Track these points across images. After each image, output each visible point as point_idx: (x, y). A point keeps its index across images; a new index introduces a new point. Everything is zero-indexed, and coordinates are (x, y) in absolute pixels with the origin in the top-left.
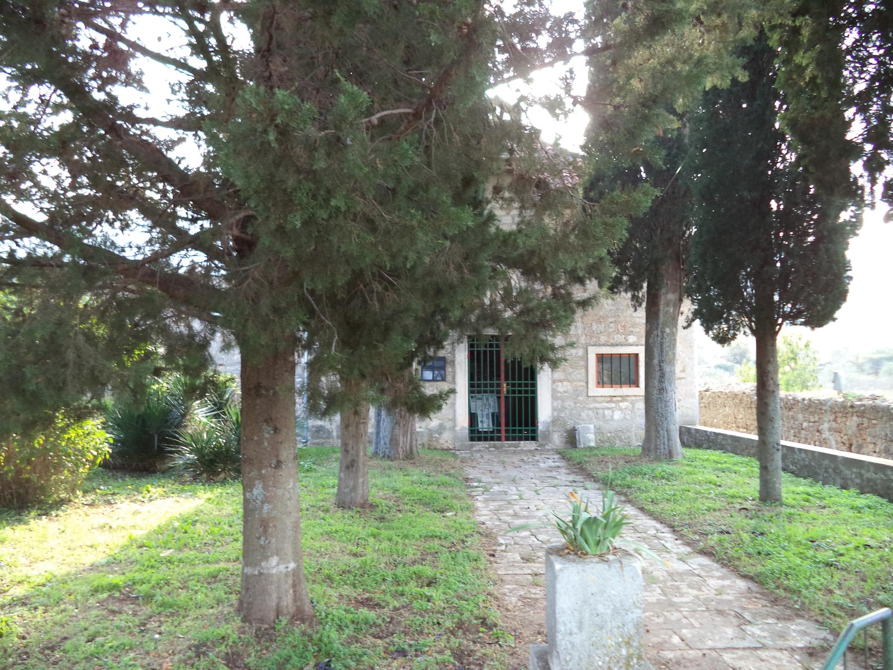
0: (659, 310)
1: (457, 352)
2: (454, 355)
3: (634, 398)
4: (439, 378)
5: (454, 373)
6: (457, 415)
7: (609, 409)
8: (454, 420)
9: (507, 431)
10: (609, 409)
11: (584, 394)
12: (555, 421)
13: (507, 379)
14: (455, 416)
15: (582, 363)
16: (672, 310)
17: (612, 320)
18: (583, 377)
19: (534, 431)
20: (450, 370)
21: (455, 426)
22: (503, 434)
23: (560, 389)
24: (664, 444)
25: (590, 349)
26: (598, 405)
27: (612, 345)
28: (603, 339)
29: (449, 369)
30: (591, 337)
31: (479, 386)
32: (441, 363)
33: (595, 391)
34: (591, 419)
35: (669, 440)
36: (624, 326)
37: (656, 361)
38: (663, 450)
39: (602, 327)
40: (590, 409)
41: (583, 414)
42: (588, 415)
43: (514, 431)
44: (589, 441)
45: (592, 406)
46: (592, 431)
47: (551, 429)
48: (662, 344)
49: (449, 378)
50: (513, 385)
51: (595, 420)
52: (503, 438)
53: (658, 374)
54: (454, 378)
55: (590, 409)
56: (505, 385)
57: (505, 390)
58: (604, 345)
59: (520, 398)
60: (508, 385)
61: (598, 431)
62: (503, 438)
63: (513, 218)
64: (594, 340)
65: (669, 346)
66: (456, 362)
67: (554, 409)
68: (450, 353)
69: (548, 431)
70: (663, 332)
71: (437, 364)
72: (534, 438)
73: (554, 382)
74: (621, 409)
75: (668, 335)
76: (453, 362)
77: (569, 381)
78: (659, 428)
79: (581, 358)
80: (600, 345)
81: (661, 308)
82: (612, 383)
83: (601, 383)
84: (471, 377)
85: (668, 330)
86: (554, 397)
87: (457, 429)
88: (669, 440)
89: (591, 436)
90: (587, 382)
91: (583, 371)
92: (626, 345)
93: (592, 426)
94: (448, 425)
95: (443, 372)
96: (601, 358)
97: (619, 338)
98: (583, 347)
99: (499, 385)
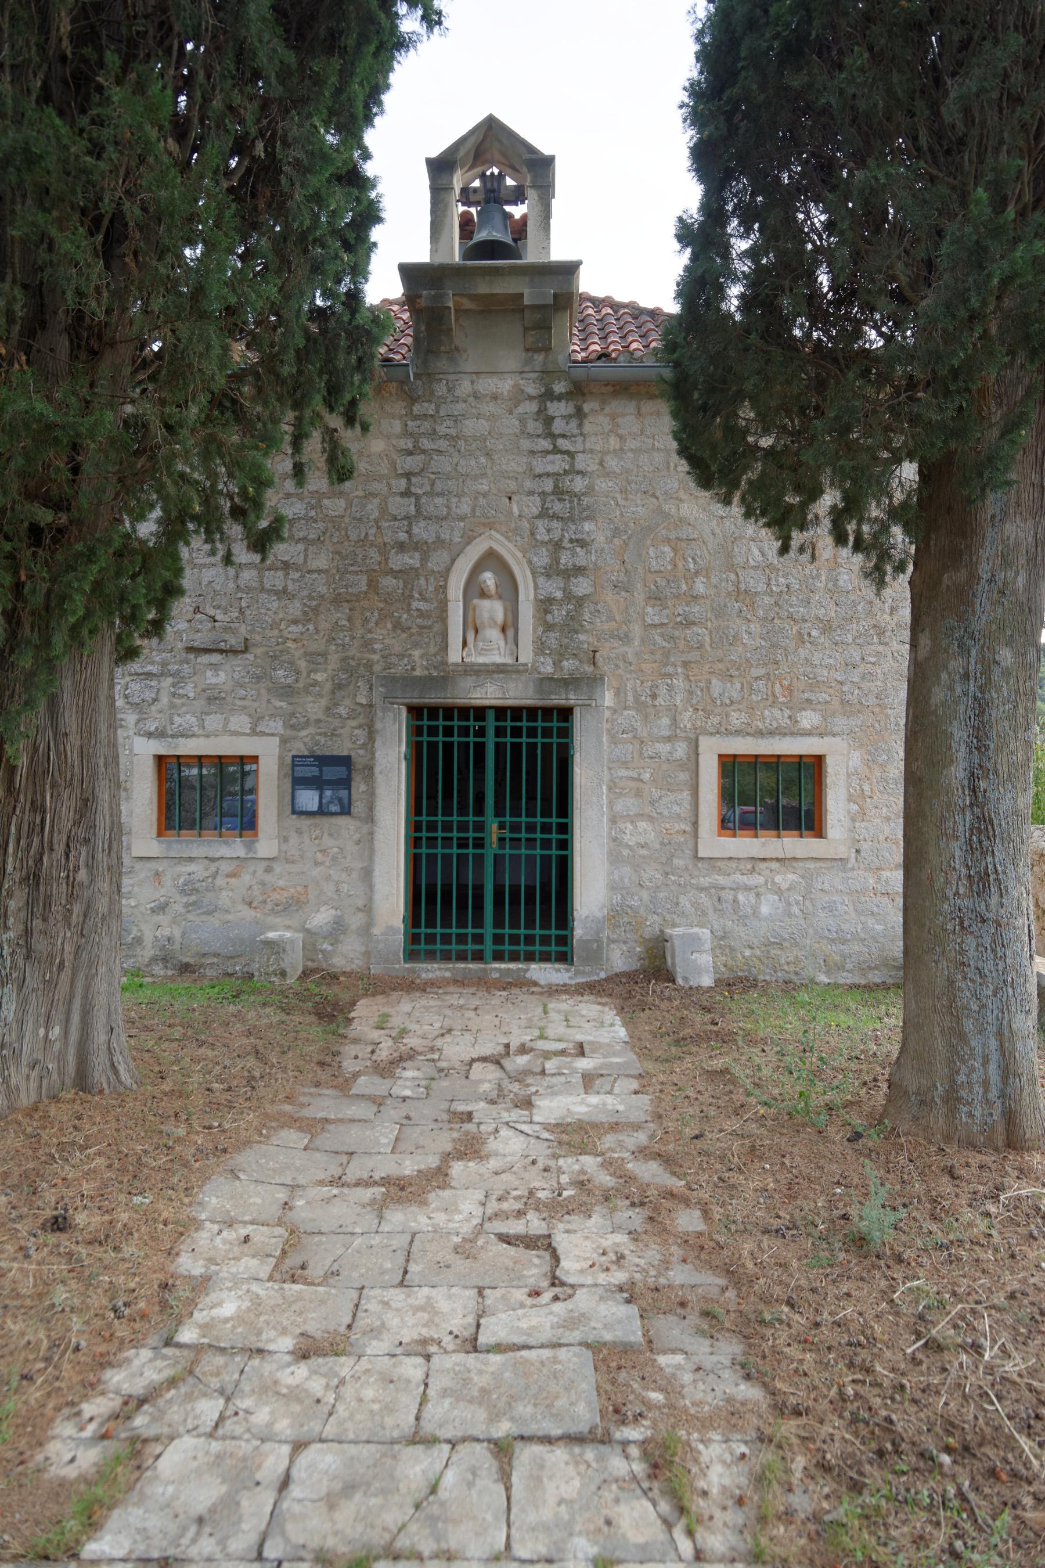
0: (973, 577)
1: (378, 743)
2: (373, 754)
3: (811, 865)
4: (334, 808)
5: (371, 794)
6: (377, 897)
7: (748, 888)
8: (368, 909)
9: (498, 939)
10: (748, 888)
11: (688, 853)
12: (615, 915)
13: (499, 812)
14: (371, 899)
15: (683, 776)
16: (1021, 582)
17: (761, 672)
18: (684, 809)
19: (564, 940)
20: (363, 787)
21: (369, 924)
22: (488, 946)
23: (629, 839)
24: (986, 1083)
25: (704, 742)
26: (721, 880)
27: (760, 734)
28: (737, 719)
29: (359, 787)
30: (708, 714)
31: (432, 827)
32: (340, 772)
33: (716, 844)
34: (704, 914)
35: (1006, 1073)
36: (790, 689)
37: (957, 773)
38: (978, 1112)
39: (734, 690)
40: (702, 889)
41: (684, 901)
42: (696, 905)
43: (514, 940)
44: (699, 970)
45: (705, 881)
46: (708, 946)
47: (604, 936)
48: (981, 707)
49: (358, 807)
50: (515, 828)
51: (712, 916)
52: (488, 954)
53: (962, 823)
54: (371, 807)
55: (702, 889)
56: (495, 827)
57: (494, 838)
58: (738, 733)
59: (531, 859)
60: (502, 826)
61: (722, 941)
62: (488, 954)
63: (523, 421)
64: (715, 720)
65: (1012, 717)
66: (377, 770)
67: (613, 887)
68: (363, 746)
69: (598, 941)
70: (988, 665)
71: (330, 773)
72: (564, 958)
73: (613, 820)
74: (779, 892)
75: (1007, 673)
76: (369, 770)
77: (651, 819)
78: (968, 1024)
79: (682, 766)
80: (729, 733)
81: (984, 571)
82: (748, 825)
83: (725, 825)
84: (416, 806)
85: (1006, 656)
86: (615, 859)
87: (376, 931)
88: (1006, 1073)
89: (705, 959)
90: (695, 824)
91: (686, 795)
92: (792, 734)
93: (705, 933)
94: (356, 921)
95: (343, 793)
96: (729, 764)
97: (779, 717)
98: (686, 739)
99: (480, 827)
